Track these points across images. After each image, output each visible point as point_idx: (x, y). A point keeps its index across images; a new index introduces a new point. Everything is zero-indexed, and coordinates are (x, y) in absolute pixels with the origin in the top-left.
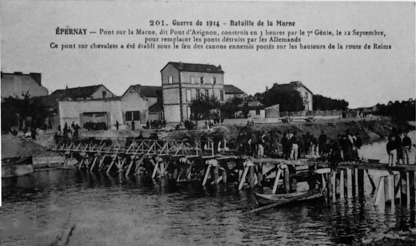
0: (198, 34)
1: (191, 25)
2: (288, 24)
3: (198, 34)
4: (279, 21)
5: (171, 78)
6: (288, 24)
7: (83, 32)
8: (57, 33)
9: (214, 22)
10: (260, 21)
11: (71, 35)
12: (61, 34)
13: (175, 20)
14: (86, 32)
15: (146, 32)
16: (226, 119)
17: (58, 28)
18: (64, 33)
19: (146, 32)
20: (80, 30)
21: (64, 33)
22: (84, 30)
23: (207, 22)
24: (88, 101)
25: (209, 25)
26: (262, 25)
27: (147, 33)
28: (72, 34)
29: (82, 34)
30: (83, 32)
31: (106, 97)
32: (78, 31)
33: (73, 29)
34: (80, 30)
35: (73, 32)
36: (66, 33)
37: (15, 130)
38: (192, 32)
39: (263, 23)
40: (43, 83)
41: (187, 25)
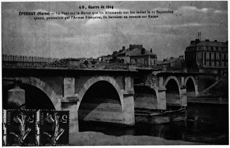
0: (60, 19)
1: (98, 8)
2: (45, 14)
3: (60, 19)
4: (40, 12)
5: (212, 58)
6: (45, 14)
7: (33, 14)
8: (19, 15)
9: (111, 6)
10: (102, 6)
11: (27, 15)
12: (22, 15)
13: (90, 6)
14: (35, 14)
15: (86, 13)
16: (133, 124)
17: (20, 12)
18: (23, 14)
19: (86, 13)
20: (32, 13)
21: (23, 14)
22: (34, 12)
23: (107, 7)
24: (174, 61)
25: (108, 8)
26: (104, 8)
27: (87, 13)
28: (28, 15)
29: (33, 15)
30: (33, 14)
31: (212, 62)
32: (31, 13)
33: (28, 12)
34: (32, 13)
35: (28, 14)
36: (24, 15)
37: (8, 64)
38: (73, 18)
39: (104, 7)
40: (210, 41)
41: (97, 8)
